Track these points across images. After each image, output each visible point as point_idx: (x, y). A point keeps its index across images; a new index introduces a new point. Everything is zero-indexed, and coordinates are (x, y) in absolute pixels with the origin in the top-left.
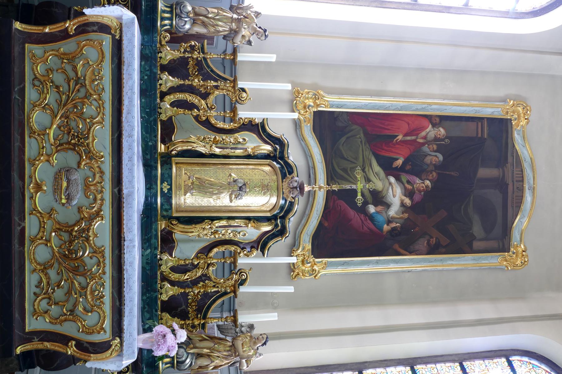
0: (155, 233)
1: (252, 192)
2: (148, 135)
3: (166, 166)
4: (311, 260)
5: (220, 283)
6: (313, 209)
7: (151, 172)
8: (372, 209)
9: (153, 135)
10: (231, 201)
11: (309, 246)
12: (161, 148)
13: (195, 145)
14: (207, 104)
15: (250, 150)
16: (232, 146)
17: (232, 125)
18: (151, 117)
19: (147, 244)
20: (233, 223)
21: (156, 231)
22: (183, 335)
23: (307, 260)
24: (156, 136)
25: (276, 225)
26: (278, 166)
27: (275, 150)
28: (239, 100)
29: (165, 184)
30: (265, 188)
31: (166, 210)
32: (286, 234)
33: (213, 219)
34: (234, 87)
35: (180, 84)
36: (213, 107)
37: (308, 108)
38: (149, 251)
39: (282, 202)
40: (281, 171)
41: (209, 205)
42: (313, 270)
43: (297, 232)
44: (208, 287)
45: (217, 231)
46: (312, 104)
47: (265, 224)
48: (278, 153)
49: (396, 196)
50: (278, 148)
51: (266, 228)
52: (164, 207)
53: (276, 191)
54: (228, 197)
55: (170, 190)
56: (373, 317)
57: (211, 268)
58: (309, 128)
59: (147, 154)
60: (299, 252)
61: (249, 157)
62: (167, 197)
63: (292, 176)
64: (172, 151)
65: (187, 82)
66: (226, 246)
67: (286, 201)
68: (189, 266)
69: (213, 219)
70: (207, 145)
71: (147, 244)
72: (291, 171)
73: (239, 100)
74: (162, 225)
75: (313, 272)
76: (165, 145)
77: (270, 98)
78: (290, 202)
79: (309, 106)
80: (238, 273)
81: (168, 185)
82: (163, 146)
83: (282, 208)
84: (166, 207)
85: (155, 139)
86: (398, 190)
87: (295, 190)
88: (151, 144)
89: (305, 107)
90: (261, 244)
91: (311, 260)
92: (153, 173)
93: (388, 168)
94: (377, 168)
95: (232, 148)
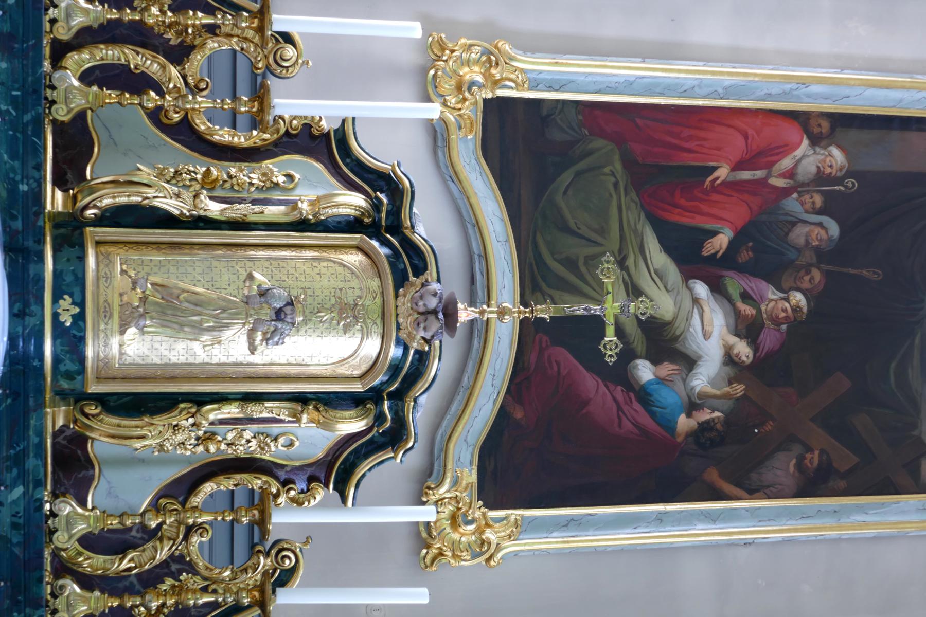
0: (35, 439)
1: (310, 325)
2: (17, 164)
3: (68, 252)
4: (478, 514)
6: (483, 372)
7: (25, 269)
9: (32, 163)
10: (253, 349)
11: (471, 476)
12: (55, 200)
13: (150, 192)
14: (184, 77)
15: (304, 207)
16: (256, 196)
17: (256, 137)
18: (25, 111)
19: (15, 471)
21: (41, 433)
23: (465, 515)
24: (40, 167)
25: (380, 418)
26: (383, 251)
27: (376, 206)
28: (274, 66)
29: (66, 302)
30: (347, 314)
31: (69, 376)
32: (407, 441)
33: (200, 400)
37: (469, 89)
38: (19, 491)
39: (395, 352)
40: (392, 265)
41: (191, 360)
42: (483, 542)
46: (480, 79)
48: (384, 215)
50: (385, 200)
51: (351, 424)
52: (62, 368)
55: (80, 318)
57: (195, 539)
58: (471, 146)
59: (14, 218)
61: (302, 225)
62: (72, 340)
63: (422, 279)
64: (86, 207)
66: (238, 476)
67: (406, 349)
68: (134, 533)
69: (200, 400)
70: (183, 191)
71: (15, 471)
72: (421, 265)
73: (274, 66)
76: (65, 191)
78: (417, 352)
79: (473, 84)
80: (273, 552)
82: (59, 194)
83: (395, 368)
87: (431, 318)
88: (25, 188)
89: (459, 88)
90: (338, 470)
91: (478, 514)
92: (32, 269)
93: (691, 258)
94: (659, 258)
95: (254, 202)
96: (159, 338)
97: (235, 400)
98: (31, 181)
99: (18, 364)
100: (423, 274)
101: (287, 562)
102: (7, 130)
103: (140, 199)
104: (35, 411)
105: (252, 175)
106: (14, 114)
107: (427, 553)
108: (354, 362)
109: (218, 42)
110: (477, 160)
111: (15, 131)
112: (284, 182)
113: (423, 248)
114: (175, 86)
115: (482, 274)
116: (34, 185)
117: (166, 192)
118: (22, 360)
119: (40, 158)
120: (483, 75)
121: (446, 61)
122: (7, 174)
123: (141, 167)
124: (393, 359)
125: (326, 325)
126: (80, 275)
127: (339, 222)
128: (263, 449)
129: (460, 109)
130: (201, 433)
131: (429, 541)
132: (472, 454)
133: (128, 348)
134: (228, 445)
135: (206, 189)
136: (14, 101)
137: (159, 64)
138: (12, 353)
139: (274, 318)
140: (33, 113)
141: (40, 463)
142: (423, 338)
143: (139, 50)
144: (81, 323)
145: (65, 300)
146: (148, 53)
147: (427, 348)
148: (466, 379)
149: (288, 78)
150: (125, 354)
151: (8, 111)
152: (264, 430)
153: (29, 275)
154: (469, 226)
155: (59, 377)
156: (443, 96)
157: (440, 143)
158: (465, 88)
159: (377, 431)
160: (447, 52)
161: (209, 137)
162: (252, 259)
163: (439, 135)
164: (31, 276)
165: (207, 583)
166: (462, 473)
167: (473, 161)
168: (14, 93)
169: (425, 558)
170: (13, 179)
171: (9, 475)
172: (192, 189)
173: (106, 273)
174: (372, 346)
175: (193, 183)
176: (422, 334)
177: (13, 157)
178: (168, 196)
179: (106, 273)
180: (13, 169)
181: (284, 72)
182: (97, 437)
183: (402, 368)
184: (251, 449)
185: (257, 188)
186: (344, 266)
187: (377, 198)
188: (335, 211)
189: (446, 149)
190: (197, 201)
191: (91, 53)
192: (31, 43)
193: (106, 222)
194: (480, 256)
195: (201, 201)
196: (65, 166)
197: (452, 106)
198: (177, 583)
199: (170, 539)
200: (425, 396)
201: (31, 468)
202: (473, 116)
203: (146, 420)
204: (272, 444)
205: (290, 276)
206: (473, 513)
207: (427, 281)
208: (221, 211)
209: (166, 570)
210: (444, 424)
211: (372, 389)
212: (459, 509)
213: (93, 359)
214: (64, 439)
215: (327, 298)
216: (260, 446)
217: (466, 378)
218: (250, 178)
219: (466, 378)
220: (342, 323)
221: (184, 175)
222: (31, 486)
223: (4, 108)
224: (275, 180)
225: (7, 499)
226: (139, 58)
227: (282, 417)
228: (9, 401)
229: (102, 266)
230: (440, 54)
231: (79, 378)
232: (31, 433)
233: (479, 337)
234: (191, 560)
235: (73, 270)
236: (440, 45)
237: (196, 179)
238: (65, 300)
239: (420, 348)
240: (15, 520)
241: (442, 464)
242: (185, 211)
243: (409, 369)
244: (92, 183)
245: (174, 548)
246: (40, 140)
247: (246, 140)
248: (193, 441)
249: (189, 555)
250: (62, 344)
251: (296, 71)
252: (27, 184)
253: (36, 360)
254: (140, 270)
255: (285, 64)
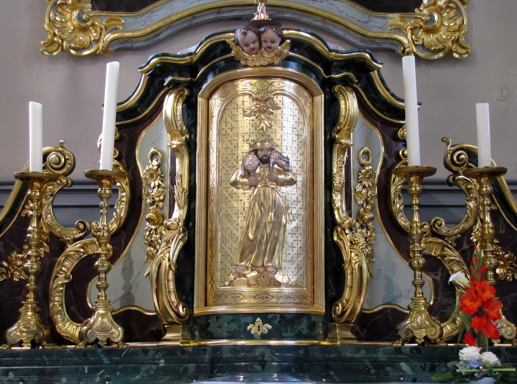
0: (363, 352)
1: (273, 135)
2: (143, 368)
3: (212, 328)
4: (425, 12)
5: (477, 208)
6: (310, 9)
7: (227, 361)
9: (142, 357)
10: (292, 182)
11: (395, 18)
12: (173, 338)
13: (165, 263)
14: (75, 240)
15: (176, 143)
16: (168, 182)
17: (123, 184)
18: (101, 362)
19: (388, 369)
20: (339, 179)
21: (358, 348)
23: (426, 22)
24: (145, 350)
25: (346, 82)
26: (210, 79)
27: (175, 85)
28: (65, 170)
29: (253, 328)
31: (312, 326)
32: (365, 59)
33: (331, 224)
34: (40, 179)
35: (35, 299)
36: (81, 226)
37: (85, 21)
38: (404, 366)
39: (292, 69)
40: (222, 70)
41: (300, 231)
42: (448, 7)
43: (362, 44)
44: (483, 234)
45: (359, 214)
46: (75, 13)
47: (343, 106)
48: (182, 79)
50: (170, 78)
51: (350, 104)
52: (305, 332)
53: (270, 81)
54: (284, 189)
55: (265, 317)
57: (444, 230)
58: (130, 20)
59: (186, 370)
60: (405, 40)
61: (191, 145)
62: (282, 324)
63: (232, 45)
64: (177, 314)
65: (31, 285)
66: (392, 196)
67: (289, 59)
68: (438, 278)
69: (331, 224)
70: (165, 238)
71: (388, 369)
72: (221, 47)
73: (65, 170)
74: (343, 337)
76: (165, 331)
78: (292, 50)
79: (79, 18)
80: (454, 168)
81: (254, 323)
82: (168, 336)
83: (305, 68)
84: (303, 326)
85: (152, 353)
87: (264, 37)
88: (162, 361)
89: (85, 30)
91: (425, 12)
92: (227, 355)
95: (173, 183)
96: (284, 256)
97: (331, 196)
98: (157, 357)
99: (302, 366)
100: (229, 45)
101: (463, 156)
102: (116, 376)
103: (171, 272)
104: (340, 353)
105: (152, 186)
106: (103, 371)
107: (456, 52)
108: (303, 102)
109: (47, 214)
110: (142, 15)
111: (116, 370)
112: (157, 161)
113: (207, 45)
114: (82, 247)
115: (233, 11)
116: (160, 354)
117: (165, 252)
118: (298, 363)
119: (138, 351)
120: (73, 10)
121: (63, 40)
122: (152, 375)
123: (147, 272)
124: (298, 70)
125: (273, 124)
126: (231, 317)
127: (188, 115)
128: (370, 176)
129: (101, 29)
130: (358, 225)
131: (446, 50)
132: (377, 17)
133: (289, 279)
134: (367, 203)
135: (163, 221)
136: (93, 372)
137: (64, 260)
138: (293, 371)
139: (267, 165)
140: (101, 356)
141: (381, 349)
142: (280, 44)
143: (53, 276)
144: (270, 317)
145: (251, 329)
146: (56, 269)
147: (289, 41)
148: (317, 23)
149: (74, 159)
150: (296, 282)
151: (101, 376)
152: (356, 175)
153: (232, 358)
154: (195, 21)
155: (313, 334)
156: (91, 42)
157: (129, 45)
158: (83, 25)
159: (357, 84)
160: (55, 39)
161: (123, 220)
162: (220, 183)
163: (122, 46)
164: (232, 355)
165: (479, 220)
166: (391, 25)
167: (143, 18)
168: (86, 371)
169: (460, 55)
170: (155, 371)
171: (391, 374)
172: (164, 233)
173: (232, 298)
174: (289, 86)
175: (158, 231)
176: (276, 45)
177: (137, 371)
178: (168, 250)
179: (232, 298)
180: (148, 371)
181: (69, 162)
182: (360, 304)
183: (306, 62)
184: (371, 185)
185: (162, 181)
186: (225, 109)
187: (168, 85)
188: (179, 118)
189: (133, 40)
190: (172, 227)
191: (57, 314)
192: (46, 359)
193: (190, 299)
194: (218, 13)
195: (172, 224)
196: (147, 332)
197: (99, 35)
198: (479, 244)
199: (443, 250)
200: (329, 44)
201: (386, 356)
202: (107, 18)
203: (346, 266)
204: (367, 168)
205: (234, 152)
206: (424, 15)
207: (234, 41)
208: (180, 208)
209: (468, 253)
211: (323, 87)
212: (421, 27)
213: (297, 307)
214: (362, 331)
215: (251, 122)
216: (369, 178)
217: (315, 23)
218: (154, 187)
219: (315, 23)
220: (271, 110)
221: (153, 239)
222: (400, 356)
223: (98, 379)
224: (156, 167)
225: (410, 375)
226: (60, 276)
227: (345, 160)
228: (332, 373)
229: (227, 301)
230: (57, 45)
231: (313, 319)
232: (357, 356)
233: (282, 12)
234: (460, 233)
235: (227, 323)
236: (50, 45)
237: (156, 230)
238: (251, 329)
239: (289, 47)
240: (427, 369)
241: (384, 41)
242: (180, 237)
243: (306, 56)
244: (158, 309)
245: (449, 246)
246: (124, 350)
247: (124, 191)
248: (364, 231)
249: (456, 234)
250: (286, 332)
251: (68, 153)
252: (159, 360)
253: (299, 352)
254: (229, 271)
255: (63, 160)
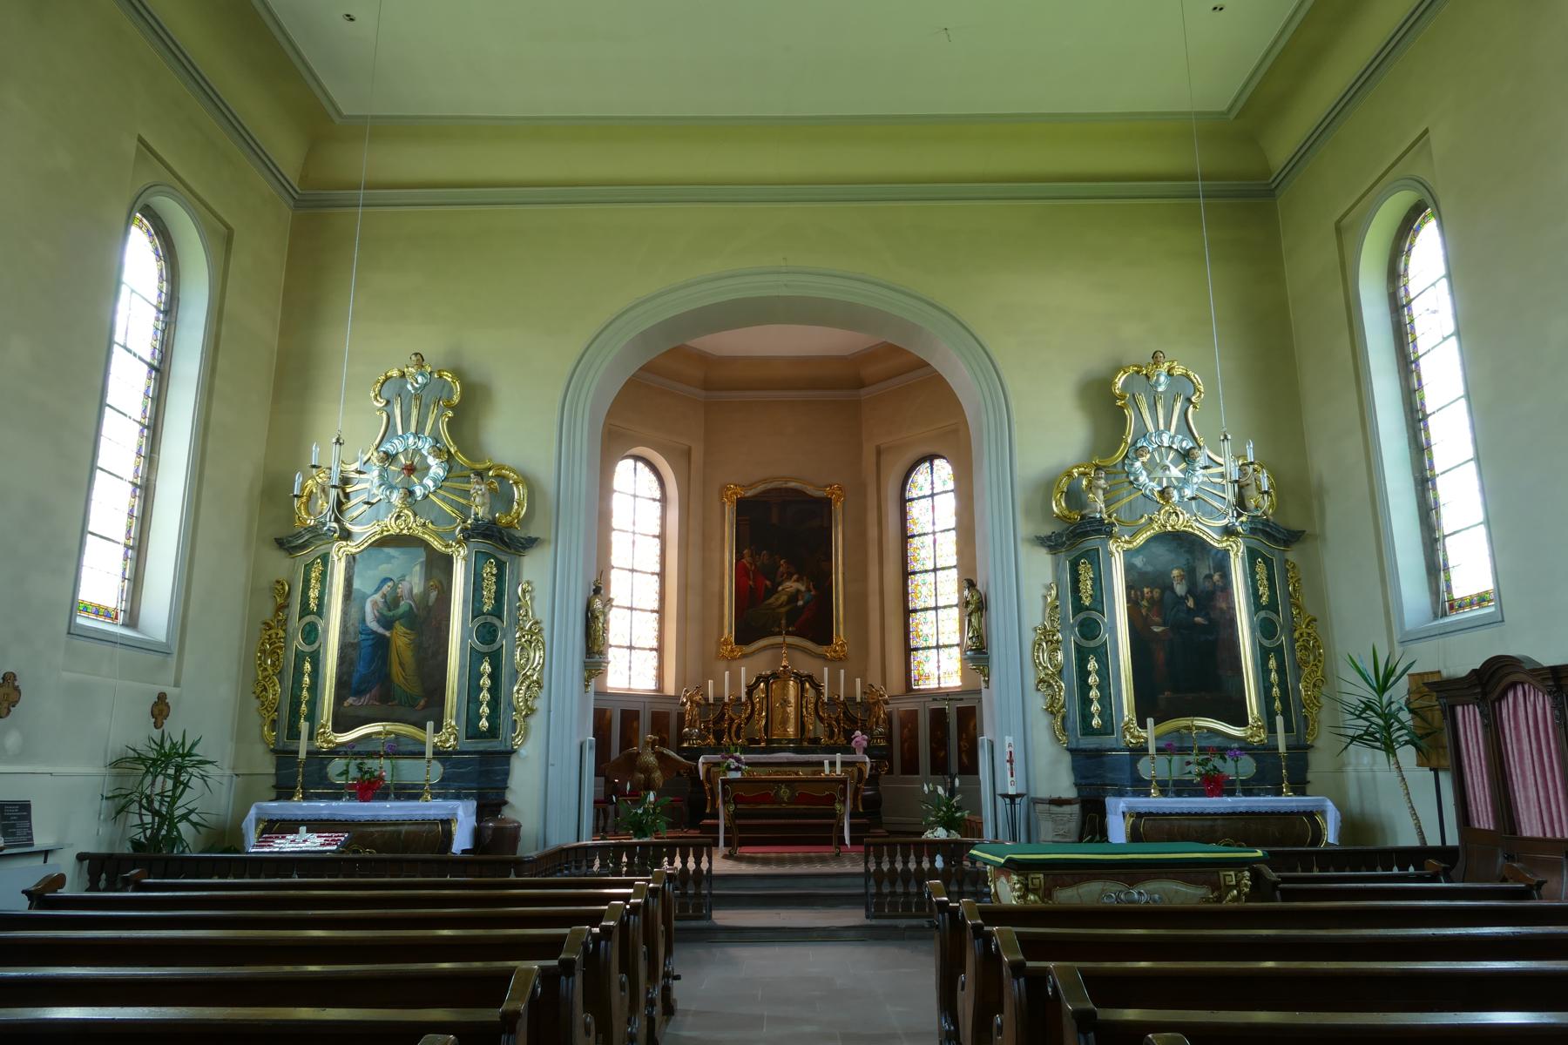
8: (800, 603)
22: (858, 733)
30: (785, 687)
49: (791, 585)
56: (874, 602)
62: (790, 741)
75: (842, 645)
77: (734, 680)
86: (788, 584)
90: (817, 687)
93: (773, 590)
94: (772, 600)
210: (1526, 747)
